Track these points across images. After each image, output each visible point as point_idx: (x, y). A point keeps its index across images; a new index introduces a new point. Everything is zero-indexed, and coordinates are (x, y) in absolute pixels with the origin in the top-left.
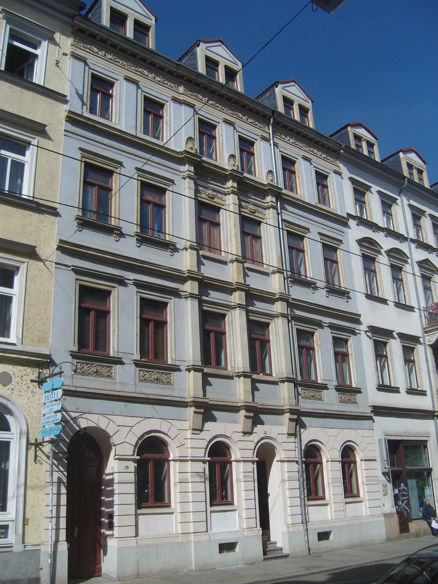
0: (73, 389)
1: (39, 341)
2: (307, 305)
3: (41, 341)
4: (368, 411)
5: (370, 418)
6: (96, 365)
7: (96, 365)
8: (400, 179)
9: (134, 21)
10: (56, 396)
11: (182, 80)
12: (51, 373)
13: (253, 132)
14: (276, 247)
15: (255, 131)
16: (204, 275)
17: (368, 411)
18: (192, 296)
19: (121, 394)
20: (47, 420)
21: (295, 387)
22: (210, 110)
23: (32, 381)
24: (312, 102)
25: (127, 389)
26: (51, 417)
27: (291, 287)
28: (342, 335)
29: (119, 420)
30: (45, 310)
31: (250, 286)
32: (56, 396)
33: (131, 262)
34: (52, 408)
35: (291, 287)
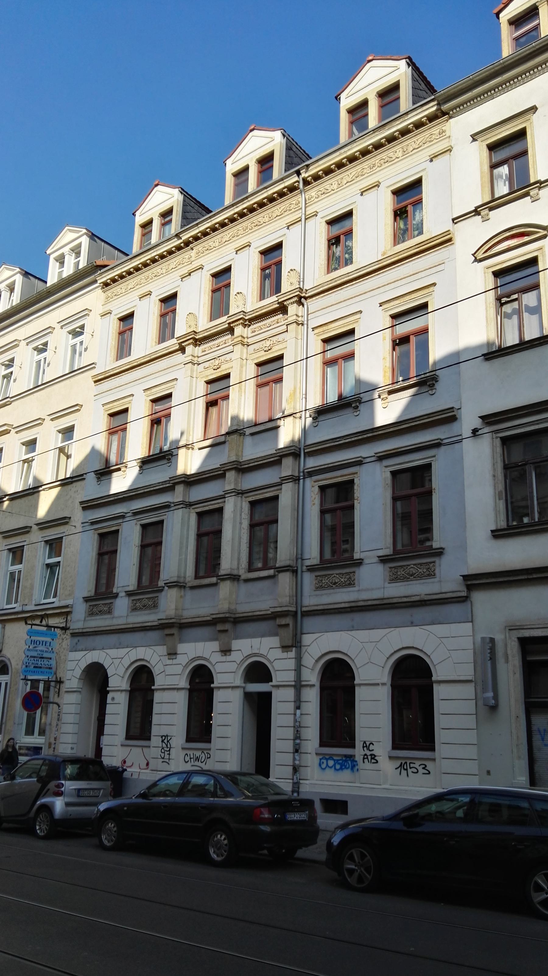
5: (464, 599)
7: (412, 566)
29: (113, 652)
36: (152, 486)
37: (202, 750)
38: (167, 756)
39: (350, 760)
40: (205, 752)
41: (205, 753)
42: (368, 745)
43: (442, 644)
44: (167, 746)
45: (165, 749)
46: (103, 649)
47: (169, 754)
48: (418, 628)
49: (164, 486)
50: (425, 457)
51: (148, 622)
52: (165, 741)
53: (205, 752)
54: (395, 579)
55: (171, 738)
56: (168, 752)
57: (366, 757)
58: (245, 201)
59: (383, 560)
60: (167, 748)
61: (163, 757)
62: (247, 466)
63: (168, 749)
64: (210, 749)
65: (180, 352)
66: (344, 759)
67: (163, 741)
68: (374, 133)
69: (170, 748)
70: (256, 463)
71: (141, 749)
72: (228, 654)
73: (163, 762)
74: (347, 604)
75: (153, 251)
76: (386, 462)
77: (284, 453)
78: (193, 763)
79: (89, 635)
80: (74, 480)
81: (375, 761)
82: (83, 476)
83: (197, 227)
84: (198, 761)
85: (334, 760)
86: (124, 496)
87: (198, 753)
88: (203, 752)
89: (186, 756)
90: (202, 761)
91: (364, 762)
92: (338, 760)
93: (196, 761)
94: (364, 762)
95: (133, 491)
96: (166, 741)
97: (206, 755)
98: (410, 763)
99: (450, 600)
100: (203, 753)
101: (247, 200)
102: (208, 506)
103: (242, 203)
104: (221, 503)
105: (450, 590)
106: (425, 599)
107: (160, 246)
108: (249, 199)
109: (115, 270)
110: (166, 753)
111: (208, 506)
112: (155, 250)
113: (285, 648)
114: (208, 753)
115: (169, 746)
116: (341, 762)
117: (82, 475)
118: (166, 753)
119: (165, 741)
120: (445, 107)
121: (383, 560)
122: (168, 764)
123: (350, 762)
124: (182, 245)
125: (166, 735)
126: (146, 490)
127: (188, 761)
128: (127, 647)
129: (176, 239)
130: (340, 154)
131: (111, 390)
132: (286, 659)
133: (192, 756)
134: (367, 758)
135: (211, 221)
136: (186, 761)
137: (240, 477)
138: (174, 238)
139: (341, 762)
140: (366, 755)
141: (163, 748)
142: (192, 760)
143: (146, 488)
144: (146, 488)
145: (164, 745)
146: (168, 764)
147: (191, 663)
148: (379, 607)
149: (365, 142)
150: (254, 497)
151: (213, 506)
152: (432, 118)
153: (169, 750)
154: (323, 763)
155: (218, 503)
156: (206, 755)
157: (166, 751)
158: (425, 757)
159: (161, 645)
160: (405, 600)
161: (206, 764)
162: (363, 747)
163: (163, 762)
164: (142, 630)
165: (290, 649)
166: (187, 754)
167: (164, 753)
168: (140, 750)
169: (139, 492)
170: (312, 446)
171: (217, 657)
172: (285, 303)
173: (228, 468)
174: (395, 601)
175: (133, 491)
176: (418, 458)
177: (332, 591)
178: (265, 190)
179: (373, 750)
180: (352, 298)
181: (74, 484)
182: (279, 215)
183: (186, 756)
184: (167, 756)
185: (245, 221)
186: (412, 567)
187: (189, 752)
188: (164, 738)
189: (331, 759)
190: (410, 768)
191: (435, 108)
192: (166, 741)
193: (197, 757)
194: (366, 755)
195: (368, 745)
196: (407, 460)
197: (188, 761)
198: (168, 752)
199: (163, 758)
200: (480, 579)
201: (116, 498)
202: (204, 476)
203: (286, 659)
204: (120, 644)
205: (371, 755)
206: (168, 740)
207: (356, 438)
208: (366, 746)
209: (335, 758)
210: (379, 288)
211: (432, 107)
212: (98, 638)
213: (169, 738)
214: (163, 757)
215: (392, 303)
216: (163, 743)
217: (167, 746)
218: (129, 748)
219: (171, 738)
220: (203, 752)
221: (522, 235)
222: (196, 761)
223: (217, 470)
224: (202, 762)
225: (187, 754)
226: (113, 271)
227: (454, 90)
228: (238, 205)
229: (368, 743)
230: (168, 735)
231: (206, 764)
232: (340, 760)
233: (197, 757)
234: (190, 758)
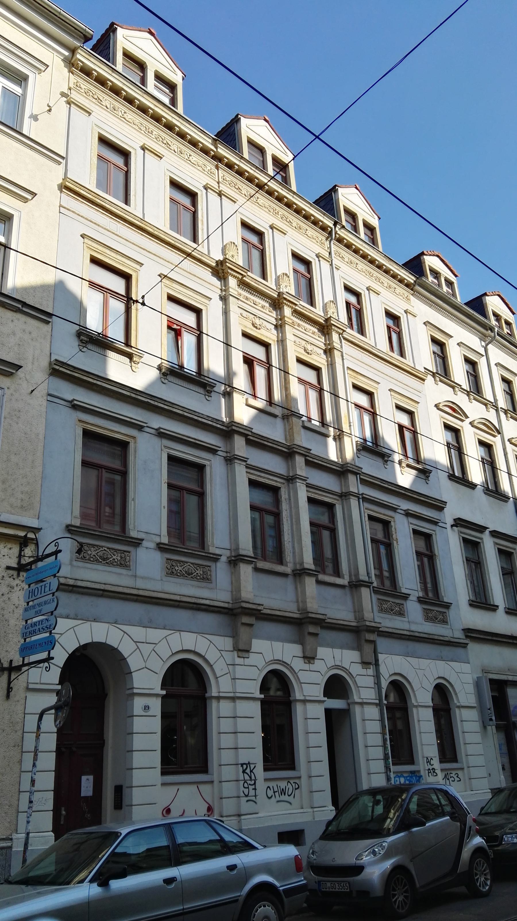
0: (71, 582)
1: (22, 507)
2: (380, 483)
3: (26, 508)
4: (459, 635)
5: (464, 646)
6: (106, 549)
7: (106, 549)
8: (487, 330)
9: (155, 73)
10: (47, 589)
11: (219, 163)
12: (40, 554)
13: (309, 248)
14: (441, 592)
15: (311, 246)
16: (253, 431)
17: (459, 635)
18: (106, 512)
19: (141, 593)
20: (31, 629)
21: (339, 335)
22: (255, 210)
23: (8, 568)
24: (380, 218)
25: (149, 586)
26: (37, 624)
27: (452, 781)
28: (426, 528)
29: (138, 632)
30: (33, 462)
31: (311, 452)
32: (47, 589)
33: (156, 404)
34: (40, 608)
35: (452, 781)
36: (197, 414)
37: (288, 779)
38: (252, 793)
39: (414, 776)
40: (292, 781)
41: (292, 783)
42: (429, 760)
43: (75, 628)
44: (250, 777)
45: (249, 782)
46: (115, 623)
47: (255, 789)
48: (444, 662)
49: (214, 424)
50: (430, 528)
51: (206, 599)
52: (246, 771)
53: (292, 781)
54: (171, 572)
55: (255, 767)
56: (253, 787)
57: (429, 771)
58: (291, 194)
59: (161, 547)
60: (251, 780)
61: (247, 794)
62: (311, 459)
63: (253, 782)
64: (299, 778)
65: (211, 270)
66: (410, 775)
67: (244, 772)
68: (384, 257)
69: (255, 780)
70: (320, 462)
71: (195, 787)
72: (312, 661)
73: (247, 801)
74: (408, 632)
75: (178, 118)
76: (412, 520)
77: (353, 470)
78: (278, 798)
79: (83, 594)
80: (24, 309)
81: (436, 774)
82: (51, 318)
83: (239, 159)
84: (285, 794)
85: (404, 777)
86: (149, 401)
87: (283, 784)
88: (289, 782)
89: (268, 789)
90: (289, 794)
91: (429, 776)
92: (407, 777)
93: (281, 794)
94: (429, 776)
95: (166, 403)
96: (248, 771)
97: (294, 785)
98: (450, 773)
99: (454, 644)
100: (289, 783)
101: (292, 195)
102: (264, 478)
103: (287, 191)
104: (279, 482)
105: (342, 618)
106: (451, 640)
107: (190, 124)
108: (295, 196)
109: (113, 74)
110: (251, 787)
111: (264, 478)
112: (180, 120)
113: (365, 664)
114: (295, 783)
115: (253, 778)
116: (408, 778)
117: (50, 315)
118: (251, 787)
119: (246, 771)
120: (418, 288)
121: (161, 547)
122: (256, 803)
123: (414, 778)
124: (212, 153)
125: (247, 763)
126: (186, 414)
127: (272, 796)
128: (164, 628)
129: (210, 141)
130: (362, 245)
131: (99, 225)
132: (365, 675)
133: (276, 789)
134: (431, 772)
135: (255, 171)
136: (270, 796)
137: (343, 479)
138: (210, 138)
139: (408, 778)
140: (429, 769)
141: (245, 782)
142: (277, 794)
143: (187, 411)
144: (187, 411)
145: (247, 777)
146: (256, 803)
147: (287, 668)
148: (426, 640)
149: (377, 256)
150: (313, 495)
151: (270, 481)
152: (408, 285)
153: (255, 784)
154: (397, 781)
155: (276, 481)
156: (294, 785)
157: (250, 784)
158: (356, 764)
159: (221, 636)
160: (441, 638)
161: (294, 797)
162: (427, 762)
163: (247, 801)
164: (191, 609)
165: (368, 666)
166: (269, 787)
167: (248, 788)
168: (194, 788)
169: (175, 410)
170: (367, 476)
171: (298, 664)
172: (333, 327)
173: (301, 452)
174: (436, 637)
175: (166, 403)
176: (428, 528)
177: (390, 617)
178: (309, 206)
179: (433, 765)
180: (371, 367)
181: (19, 316)
182: (309, 235)
183: (268, 789)
184: (252, 793)
185: (278, 206)
186: (105, 550)
187: (271, 784)
188: (245, 766)
189: (402, 777)
190: (451, 777)
191: (412, 282)
192: (248, 771)
193: (283, 789)
194: (429, 769)
195: (429, 760)
196: (422, 525)
197: (272, 796)
198: (253, 787)
199: (247, 796)
200: (472, 633)
201: (133, 395)
202: (266, 443)
203: (365, 675)
204: (150, 621)
205: (433, 769)
206: (251, 769)
207: (394, 489)
208: (429, 762)
209: (405, 775)
210: (387, 375)
211: (412, 279)
212: (103, 604)
213: (252, 766)
214: (247, 794)
215: (405, 399)
216: (245, 774)
217: (250, 777)
218: (175, 788)
219: (255, 767)
220: (289, 782)
221: (454, 410)
222: (281, 794)
223: (282, 445)
224: (289, 796)
225: (269, 787)
226: (110, 72)
227: (440, 293)
228: (284, 189)
229: (429, 759)
230: (251, 762)
231: (294, 797)
232: (408, 776)
233: (283, 789)
234: (274, 792)
